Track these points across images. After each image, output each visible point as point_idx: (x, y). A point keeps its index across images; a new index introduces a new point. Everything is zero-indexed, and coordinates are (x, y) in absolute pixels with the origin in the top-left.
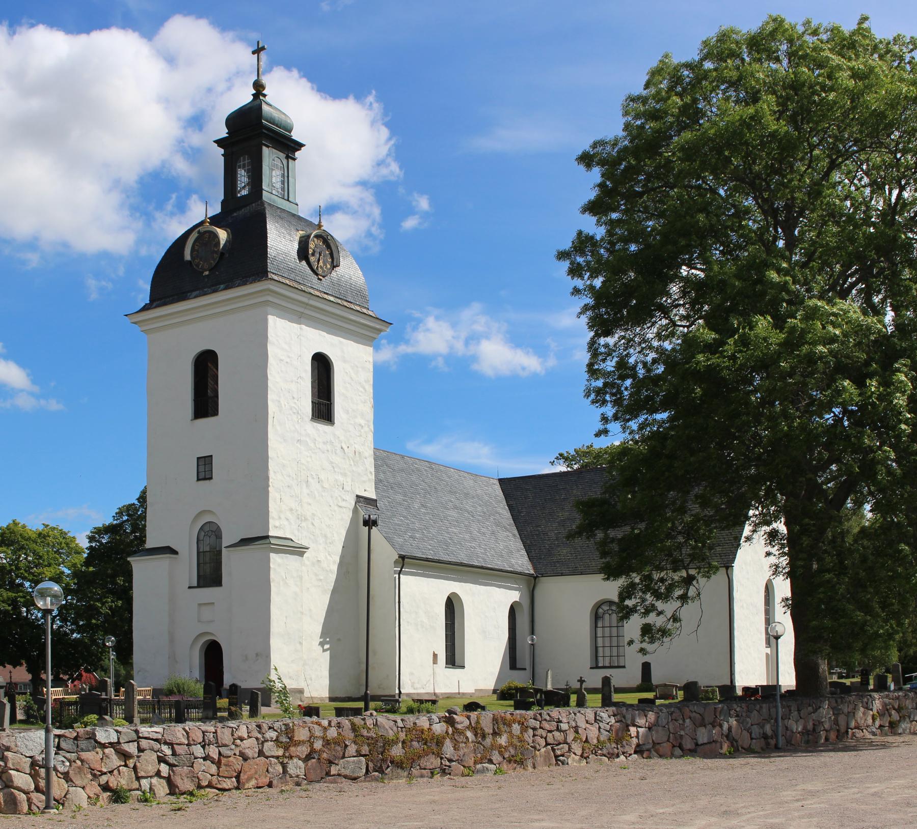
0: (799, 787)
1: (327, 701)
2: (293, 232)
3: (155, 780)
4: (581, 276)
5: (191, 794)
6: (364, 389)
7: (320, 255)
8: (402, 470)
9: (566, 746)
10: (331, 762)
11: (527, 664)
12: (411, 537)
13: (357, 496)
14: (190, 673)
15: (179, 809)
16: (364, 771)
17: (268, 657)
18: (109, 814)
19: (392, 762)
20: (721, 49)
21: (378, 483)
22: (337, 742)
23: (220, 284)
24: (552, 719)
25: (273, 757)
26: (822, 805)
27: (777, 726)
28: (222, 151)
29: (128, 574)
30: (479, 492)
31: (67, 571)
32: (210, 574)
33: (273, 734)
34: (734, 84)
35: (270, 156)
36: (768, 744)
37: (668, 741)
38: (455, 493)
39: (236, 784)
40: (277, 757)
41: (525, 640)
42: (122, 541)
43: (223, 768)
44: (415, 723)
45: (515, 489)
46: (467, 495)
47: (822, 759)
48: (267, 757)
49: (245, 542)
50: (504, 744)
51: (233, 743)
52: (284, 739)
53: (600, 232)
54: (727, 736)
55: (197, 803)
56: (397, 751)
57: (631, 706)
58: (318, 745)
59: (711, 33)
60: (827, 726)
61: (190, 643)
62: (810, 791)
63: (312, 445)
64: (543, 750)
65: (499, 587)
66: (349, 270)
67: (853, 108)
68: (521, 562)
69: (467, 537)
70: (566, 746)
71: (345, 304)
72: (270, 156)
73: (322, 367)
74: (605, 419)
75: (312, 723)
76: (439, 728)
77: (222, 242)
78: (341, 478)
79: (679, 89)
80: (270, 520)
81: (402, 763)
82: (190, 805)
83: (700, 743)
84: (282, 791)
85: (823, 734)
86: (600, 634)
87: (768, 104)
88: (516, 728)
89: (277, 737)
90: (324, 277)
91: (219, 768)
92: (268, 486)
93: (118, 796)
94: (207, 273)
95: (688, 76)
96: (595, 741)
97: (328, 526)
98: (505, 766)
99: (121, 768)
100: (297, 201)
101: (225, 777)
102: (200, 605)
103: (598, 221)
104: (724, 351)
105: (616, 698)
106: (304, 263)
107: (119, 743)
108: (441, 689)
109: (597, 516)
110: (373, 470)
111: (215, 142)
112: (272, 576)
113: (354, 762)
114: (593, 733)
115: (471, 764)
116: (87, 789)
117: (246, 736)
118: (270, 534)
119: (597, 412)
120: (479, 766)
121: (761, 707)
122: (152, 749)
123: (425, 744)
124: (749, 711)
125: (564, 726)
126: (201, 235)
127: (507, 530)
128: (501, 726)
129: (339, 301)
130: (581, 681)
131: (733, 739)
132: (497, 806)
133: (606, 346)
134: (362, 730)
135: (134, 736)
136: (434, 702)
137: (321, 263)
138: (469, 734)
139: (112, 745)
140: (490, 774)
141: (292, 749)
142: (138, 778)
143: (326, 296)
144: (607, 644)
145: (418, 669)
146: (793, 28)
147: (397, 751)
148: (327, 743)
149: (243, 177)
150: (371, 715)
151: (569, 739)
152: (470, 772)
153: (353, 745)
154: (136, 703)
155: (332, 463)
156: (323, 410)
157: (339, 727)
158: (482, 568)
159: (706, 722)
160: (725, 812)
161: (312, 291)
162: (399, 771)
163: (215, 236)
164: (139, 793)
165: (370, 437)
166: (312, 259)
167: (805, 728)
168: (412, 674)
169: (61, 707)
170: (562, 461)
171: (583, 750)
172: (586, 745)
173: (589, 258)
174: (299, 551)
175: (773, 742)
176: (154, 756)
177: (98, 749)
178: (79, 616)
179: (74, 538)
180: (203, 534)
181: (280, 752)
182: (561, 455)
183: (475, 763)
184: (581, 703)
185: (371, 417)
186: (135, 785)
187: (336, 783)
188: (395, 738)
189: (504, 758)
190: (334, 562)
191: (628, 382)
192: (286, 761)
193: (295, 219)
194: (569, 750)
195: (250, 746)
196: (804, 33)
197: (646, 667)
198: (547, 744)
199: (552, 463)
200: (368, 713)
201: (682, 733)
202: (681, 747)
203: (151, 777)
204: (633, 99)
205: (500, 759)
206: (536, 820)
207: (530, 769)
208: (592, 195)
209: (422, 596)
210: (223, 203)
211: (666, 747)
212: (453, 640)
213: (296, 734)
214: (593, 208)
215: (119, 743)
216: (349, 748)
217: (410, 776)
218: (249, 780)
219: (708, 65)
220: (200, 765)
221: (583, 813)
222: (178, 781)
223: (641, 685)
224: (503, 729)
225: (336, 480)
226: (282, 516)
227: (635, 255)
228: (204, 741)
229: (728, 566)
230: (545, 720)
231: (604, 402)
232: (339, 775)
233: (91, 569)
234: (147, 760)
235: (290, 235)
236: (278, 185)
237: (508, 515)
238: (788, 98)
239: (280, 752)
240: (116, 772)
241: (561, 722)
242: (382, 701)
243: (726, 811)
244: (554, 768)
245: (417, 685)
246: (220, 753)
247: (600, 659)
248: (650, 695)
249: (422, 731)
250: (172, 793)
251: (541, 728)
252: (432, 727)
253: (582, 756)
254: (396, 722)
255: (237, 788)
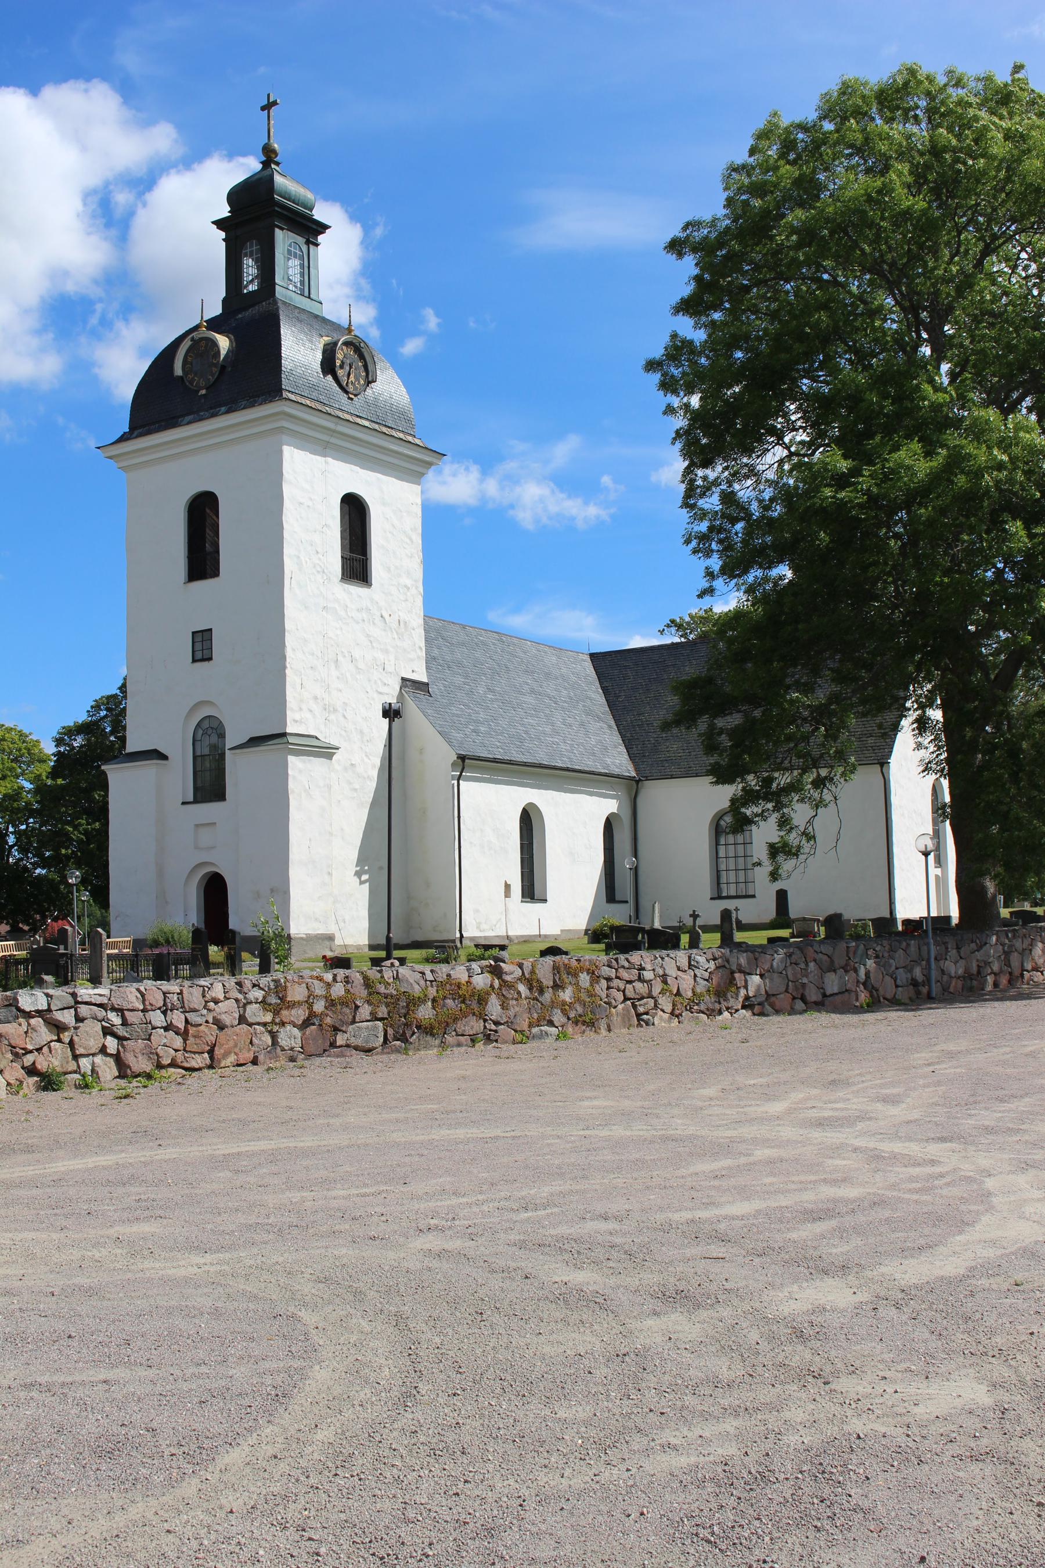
0: (938, 1048)
1: (367, 950)
2: (315, 339)
3: (99, 1059)
4: (675, 392)
5: (149, 1076)
6: (411, 539)
7: (351, 367)
8: (463, 644)
9: (651, 1002)
10: (336, 1029)
11: (630, 896)
12: (474, 731)
13: (403, 679)
14: (185, 916)
15: (126, 1097)
16: (381, 1039)
17: (287, 893)
18: (31, 1107)
19: (419, 1027)
20: (845, 105)
21: (430, 661)
22: (344, 1002)
23: (221, 406)
24: (632, 966)
25: (258, 1024)
26: (958, 1070)
27: (930, 968)
28: (223, 235)
29: (105, 786)
30: (564, 671)
31: (28, 786)
32: (210, 785)
33: (259, 994)
34: (859, 151)
35: (283, 240)
36: (918, 993)
37: (787, 991)
38: (533, 672)
39: (208, 1061)
40: (264, 1024)
41: (625, 863)
42: (98, 743)
43: (191, 1040)
44: (449, 975)
45: (610, 666)
46: (548, 675)
47: (981, 1010)
48: (250, 1025)
49: (256, 741)
50: (568, 1000)
51: (205, 1007)
52: (273, 1000)
53: (699, 336)
54: (864, 984)
55: (154, 1087)
56: (425, 1013)
57: (761, 946)
58: (319, 1007)
59: (833, 86)
60: (996, 967)
61: (185, 876)
62: (950, 1052)
63: (342, 613)
64: (620, 1007)
65: (591, 794)
66: (389, 386)
67: (1008, 179)
68: (619, 761)
69: (548, 729)
70: (651, 1002)
71: (384, 430)
72: (283, 240)
73: (354, 510)
74: (710, 574)
75: (311, 977)
76: (482, 981)
77: (223, 353)
78: (380, 656)
79: (792, 156)
80: (288, 713)
81: (432, 1028)
82: (142, 1090)
83: (828, 993)
84: (269, 1069)
85: (990, 979)
86: (722, 854)
87: (900, 173)
88: (584, 979)
89: (264, 997)
90: (356, 395)
91: (185, 1040)
92: (285, 667)
93: (48, 1082)
94: (203, 392)
95: (803, 141)
96: (690, 994)
97: (365, 719)
98: (570, 1029)
99: (52, 1044)
100: (321, 299)
101: (195, 1053)
102: (197, 826)
103: (696, 323)
104: (859, 483)
105: (739, 937)
106: (330, 378)
107: (49, 1010)
108: (515, 932)
109: (700, 699)
110: (423, 644)
111: (213, 223)
112: (291, 785)
113: (367, 1028)
114: (686, 983)
115: (525, 1027)
116: (6, 1074)
117: (221, 997)
118: (289, 730)
119: (699, 564)
120: (535, 1030)
121: (908, 945)
122: (95, 1018)
123: (463, 1002)
124: (892, 950)
125: (648, 975)
126: (195, 344)
127: (600, 719)
128: (565, 976)
129: (376, 427)
130: (695, 916)
131: (873, 987)
132: (544, 1080)
133: (705, 478)
134: (378, 986)
135: (71, 1001)
136: (503, 948)
137: (352, 378)
138: (522, 988)
139: (39, 1013)
140: (549, 1040)
141: (284, 1013)
142: (76, 1057)
143: (359, 421)
144: (732, 867)
145: (487, 906)
146: (930, 79)
147: (425, 1013)
148: (331, 1003)
149: (250, 268)
150: (392, 965)
151: (656, 992)
152: (523, 1037)
153: (366, 1006)
154: (105, 958)
155: (368, 636)
156: (357, 566)
157: (347, 982)
158: (567, 769)
159: (837, 965)
160: (833, 1082)
161: (340, 414)
162: (429, 1038)
163: (214, 344)
164: (77, 1076)
165: (419, 601)
166: (340, 373)
167: (966, 971)
168: (477, 911)
169: (7, 967)
170: (673, 630)
171: (674, 1005)
172: (677, 998)
173: (687, 369)
174: (327, 752)
175: (924, 990)
176: (98, 1027)
177: (21, 1020)
178: (43, 845)
179: (38, 741)
180: (200, 732)
181: (268, 1018)
182: (673, 621)
183: (531, 1026)
184: (694, 943)
185: (418, 573)
186: (73, 1065)
187: (344, 1056)
188: (422, 996)
189: (569, 1019)
190: (374, 766)
191: (739, 526)
192: (276, 1028)
193: (318, 322)
194: (656, 1006)
195: (227, 1011)
196: (945, 85)
197: (782, 897)
198: (626, 999)
199: (662, 632)
200: (388, 963)
201: (805, 980)
202: (803, 999)
203: (93, 1055)
204: (735, 169)
205: (564, 1020)
206: (587, 1098)
207: (603, 1031)
208: (687, 290)
209: (489, 810)
210: (224, 301)
211: (783, 1000)
212: (532, 864)
213: (290, 993)
214: (688, 306)
215: (49, 1010)
216: (360, 1010)
217: (443, 1045)
218: (226, 1055)
219: (828, 126)
220: (160, 1037)
221: (652, 1087)
222: (129, 1059)
223: (775, 919)
224: (566, 980)
225: (375, 659)
226: (304, 707)
227: (744, 365)
228: (165, 1004)
229: (883, 763)
230: (623, 967)
231: (708, 553)
232: (348, 1046)
233: (60, 781)
234: (87, 1032)
235: (311, 342)
236: (297, 279)
237: (603, 700)
238: (928, 167)
239: (268, 1018)
240: (45, 1049)
241: (644, 969)
242: (437, 947)
243: (834, 1081)
244: (635, 1030)
245: (484, 926)
246: (187, 1021)
247: (724, 887)
248: (784, 933)
249: (459, 986)
250: (122, 1076)
251: (617, 977)
252: (472, 979)
253: (672, 1013)
254: (423, 973)
255: (211, 1067)
